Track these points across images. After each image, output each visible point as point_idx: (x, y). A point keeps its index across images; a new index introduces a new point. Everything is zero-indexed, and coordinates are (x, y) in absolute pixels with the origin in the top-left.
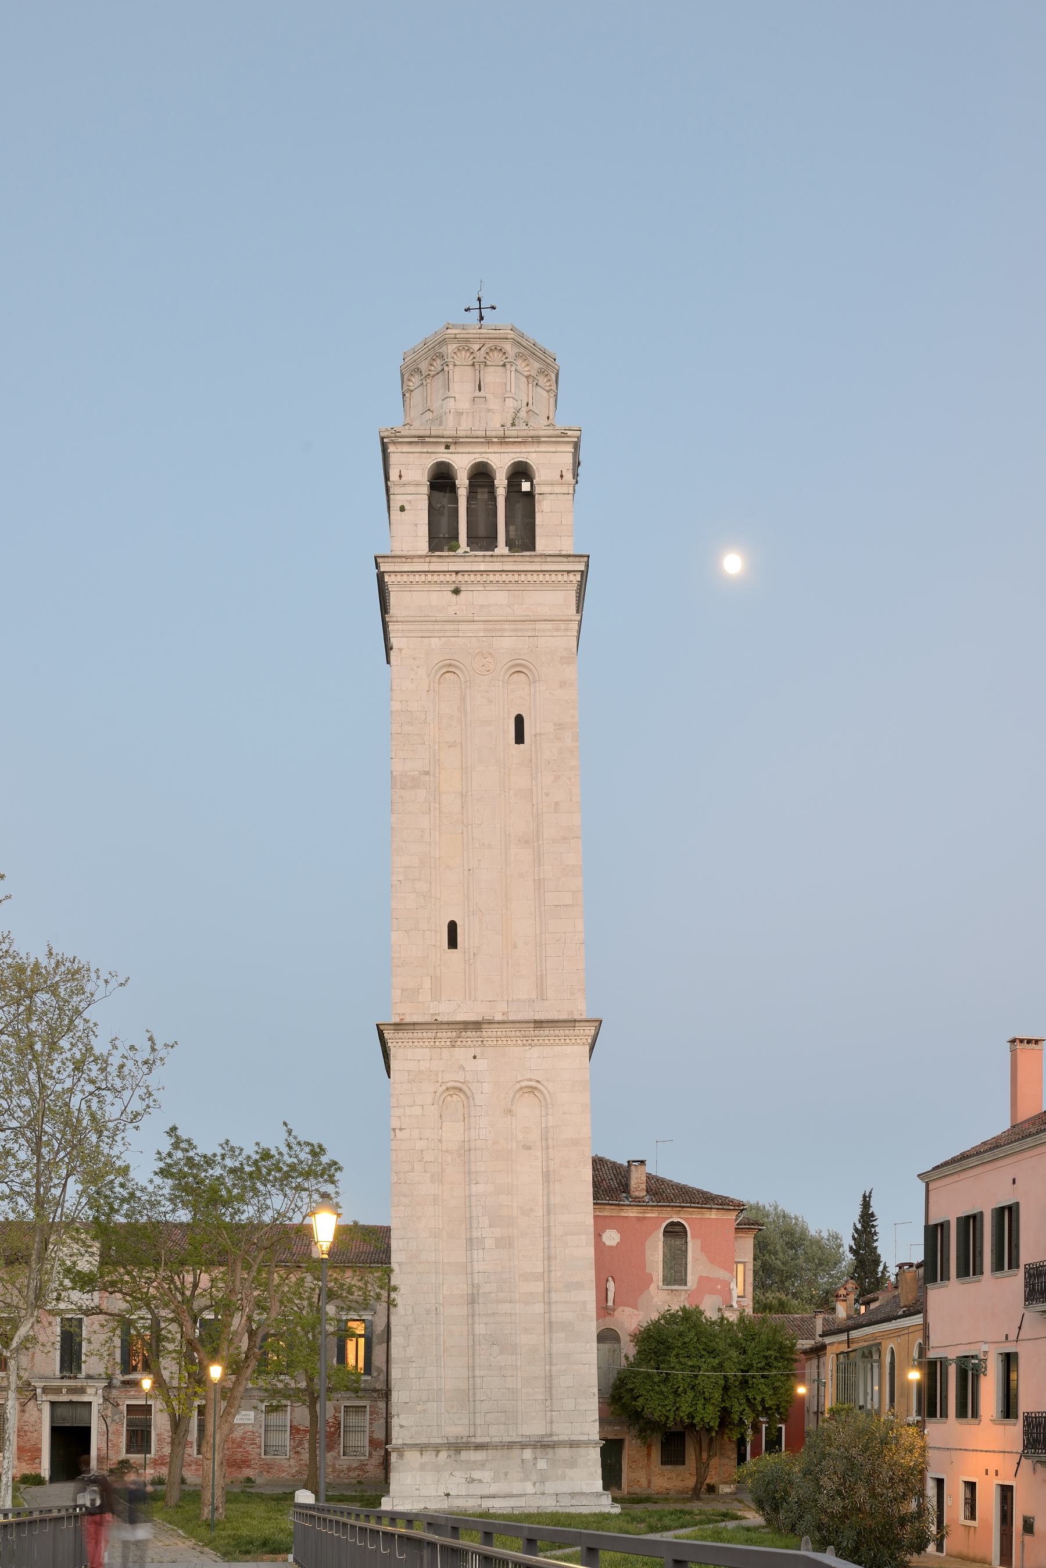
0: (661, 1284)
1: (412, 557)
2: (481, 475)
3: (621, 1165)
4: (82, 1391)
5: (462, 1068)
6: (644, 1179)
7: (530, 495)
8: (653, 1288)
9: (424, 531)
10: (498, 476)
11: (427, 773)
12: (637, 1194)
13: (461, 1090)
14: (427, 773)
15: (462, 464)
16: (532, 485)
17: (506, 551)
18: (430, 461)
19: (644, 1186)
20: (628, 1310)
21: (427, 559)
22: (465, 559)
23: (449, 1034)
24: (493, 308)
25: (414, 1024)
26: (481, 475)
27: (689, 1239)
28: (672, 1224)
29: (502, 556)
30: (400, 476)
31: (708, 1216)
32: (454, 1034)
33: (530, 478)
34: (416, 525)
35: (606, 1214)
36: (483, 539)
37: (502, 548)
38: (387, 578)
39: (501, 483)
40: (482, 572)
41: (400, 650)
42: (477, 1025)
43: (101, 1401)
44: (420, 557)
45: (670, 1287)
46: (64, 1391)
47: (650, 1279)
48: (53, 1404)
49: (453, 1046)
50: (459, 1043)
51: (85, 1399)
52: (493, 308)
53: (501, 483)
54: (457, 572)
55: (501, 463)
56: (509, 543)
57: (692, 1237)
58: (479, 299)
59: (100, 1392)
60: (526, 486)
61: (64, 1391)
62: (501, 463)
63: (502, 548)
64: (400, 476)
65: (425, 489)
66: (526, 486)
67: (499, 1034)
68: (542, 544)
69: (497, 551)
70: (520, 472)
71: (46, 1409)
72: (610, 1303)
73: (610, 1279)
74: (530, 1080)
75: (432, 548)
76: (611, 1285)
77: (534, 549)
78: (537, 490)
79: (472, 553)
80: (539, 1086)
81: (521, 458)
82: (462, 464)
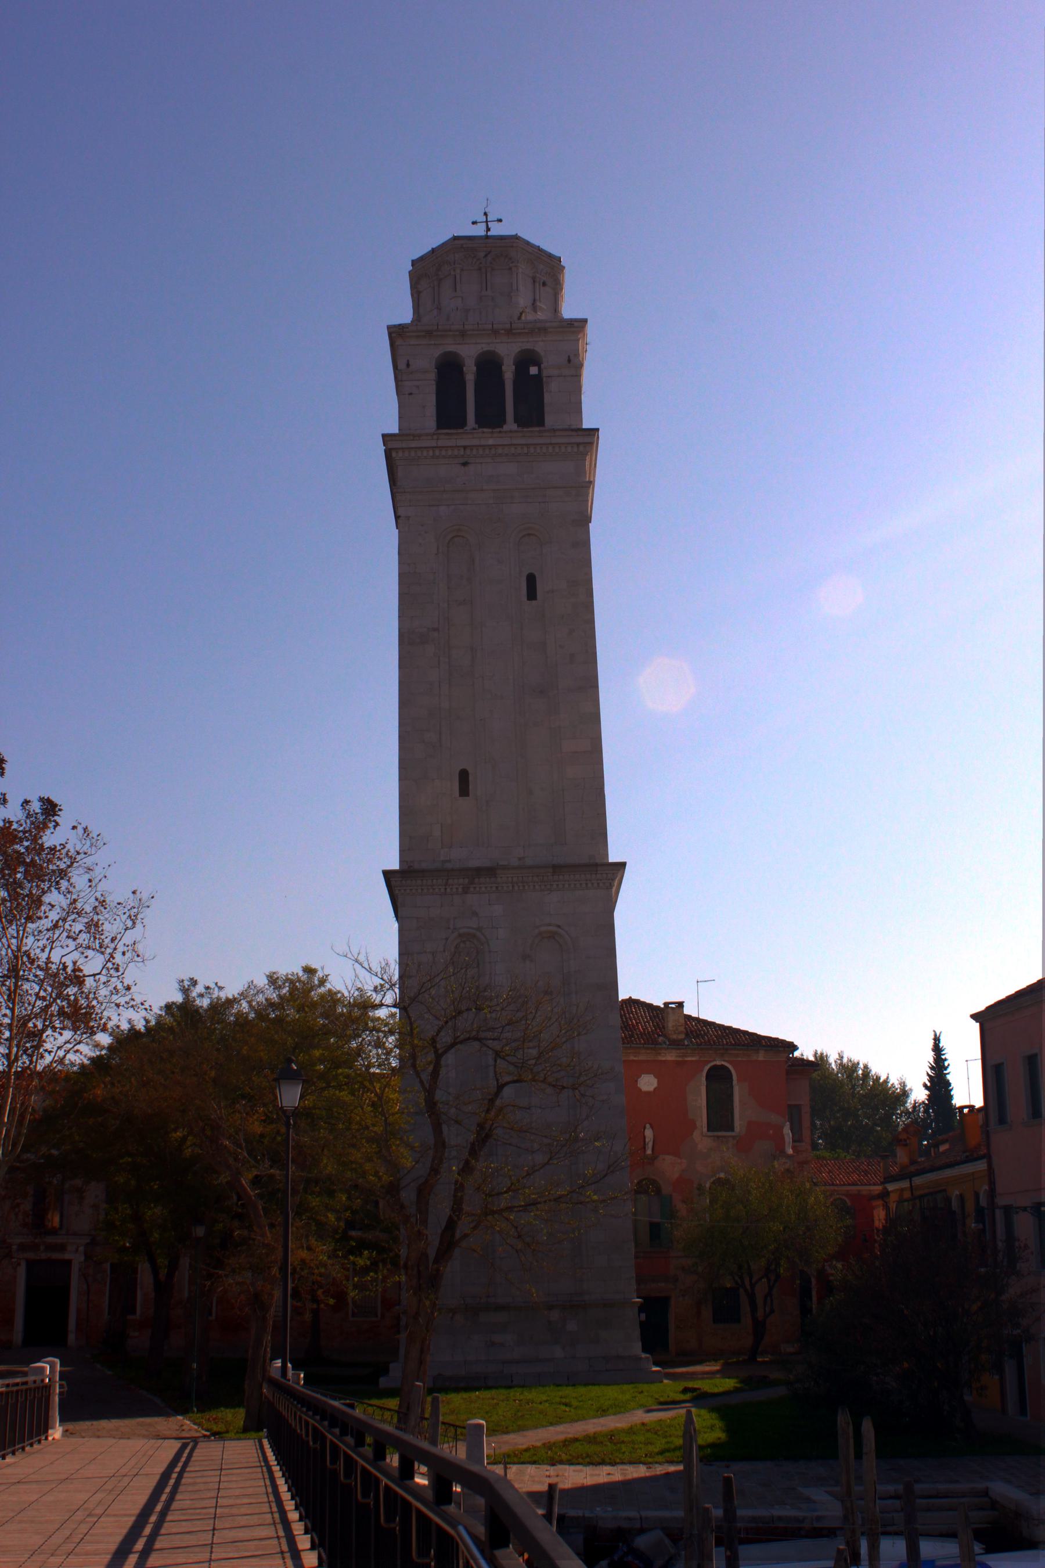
0: (705, 1130)
1: (420, 436)
2: (489, 365)
3: (658, 1007)
4: (62, 1248)
5: (475, 914)
6: (682, 1021)
7: (538, 378)
8: (696, 1134)
9: (431, 410)
10: (506, 362)
11: (435, 630)
12: (675, 1037)
13: (529, 535)
14: (435, 630)
15: (469, 353)
16: (540, 370)
17: (515, 427)
18: (437, 353)
19: (682, 1029)
20: (669, 1159)
21: (435, 437)
22: (473, 436)
23: (461, 881)
24: (500, 221)
25: (423, 871)
26: (489, 365)
27: (735, 1082)
28: (715, 1068)
29: (511, 431)
30: (408, 365)
31: (754, 1058)
32: (466, 881)
33: (538, 363)
34: (424, 407)
35: (642, 1058)
36: (490, 417)
37: (510, 425)
38: (394, 454)
39: (509, 373)
40: (490, 447)
41: (408, 518)
42: (490, 871)
43: (82, 1258)
44: (427, 435)
45: (716, 1133)
46: (42, 1248)
47: (693, 1125)
48: (30, 1264)
49: (466, 893)
50: (472, 889)
51: (67, 1256)
52: (500, 221)
53: (509, 373)
54: (465, 447)
55: (508, 351)
56: (517, 420)
57: (739, 1080)
58: (486, 214)
59: (81, 1249)
60: (533, 370)
61: (42, 1248)
62: (508, 351)
63: (510, 425)
64: (408, 365)
65: (433, 375)
66: (533, 370)
67: (515, 879)
68: (549, 420)
69: (505, 428)
70: (526, 360)
71: (22, 1270)
72: (649, 1152)
73: (648, 1126)
74: (550, 925)
75: (440, 426)
76: (649, 1133)
77: (541, 422)
78: (545, 373)
79: (481, 430)
80: (560, 930)
81: (528, 346)
82: (469, 353)
